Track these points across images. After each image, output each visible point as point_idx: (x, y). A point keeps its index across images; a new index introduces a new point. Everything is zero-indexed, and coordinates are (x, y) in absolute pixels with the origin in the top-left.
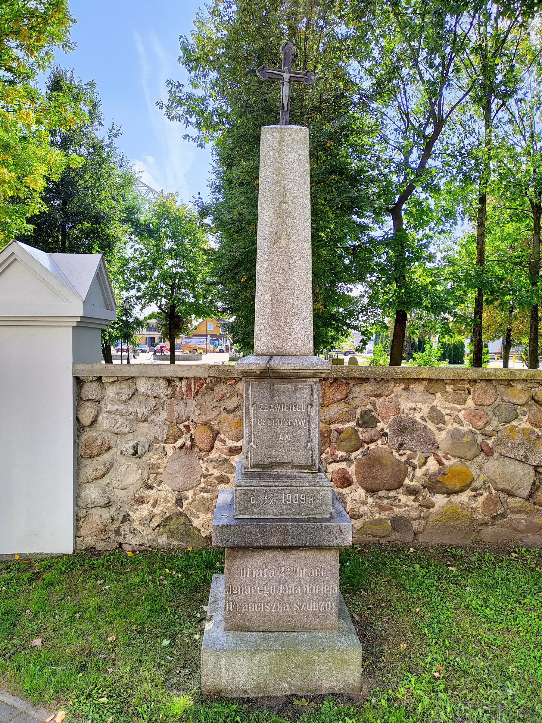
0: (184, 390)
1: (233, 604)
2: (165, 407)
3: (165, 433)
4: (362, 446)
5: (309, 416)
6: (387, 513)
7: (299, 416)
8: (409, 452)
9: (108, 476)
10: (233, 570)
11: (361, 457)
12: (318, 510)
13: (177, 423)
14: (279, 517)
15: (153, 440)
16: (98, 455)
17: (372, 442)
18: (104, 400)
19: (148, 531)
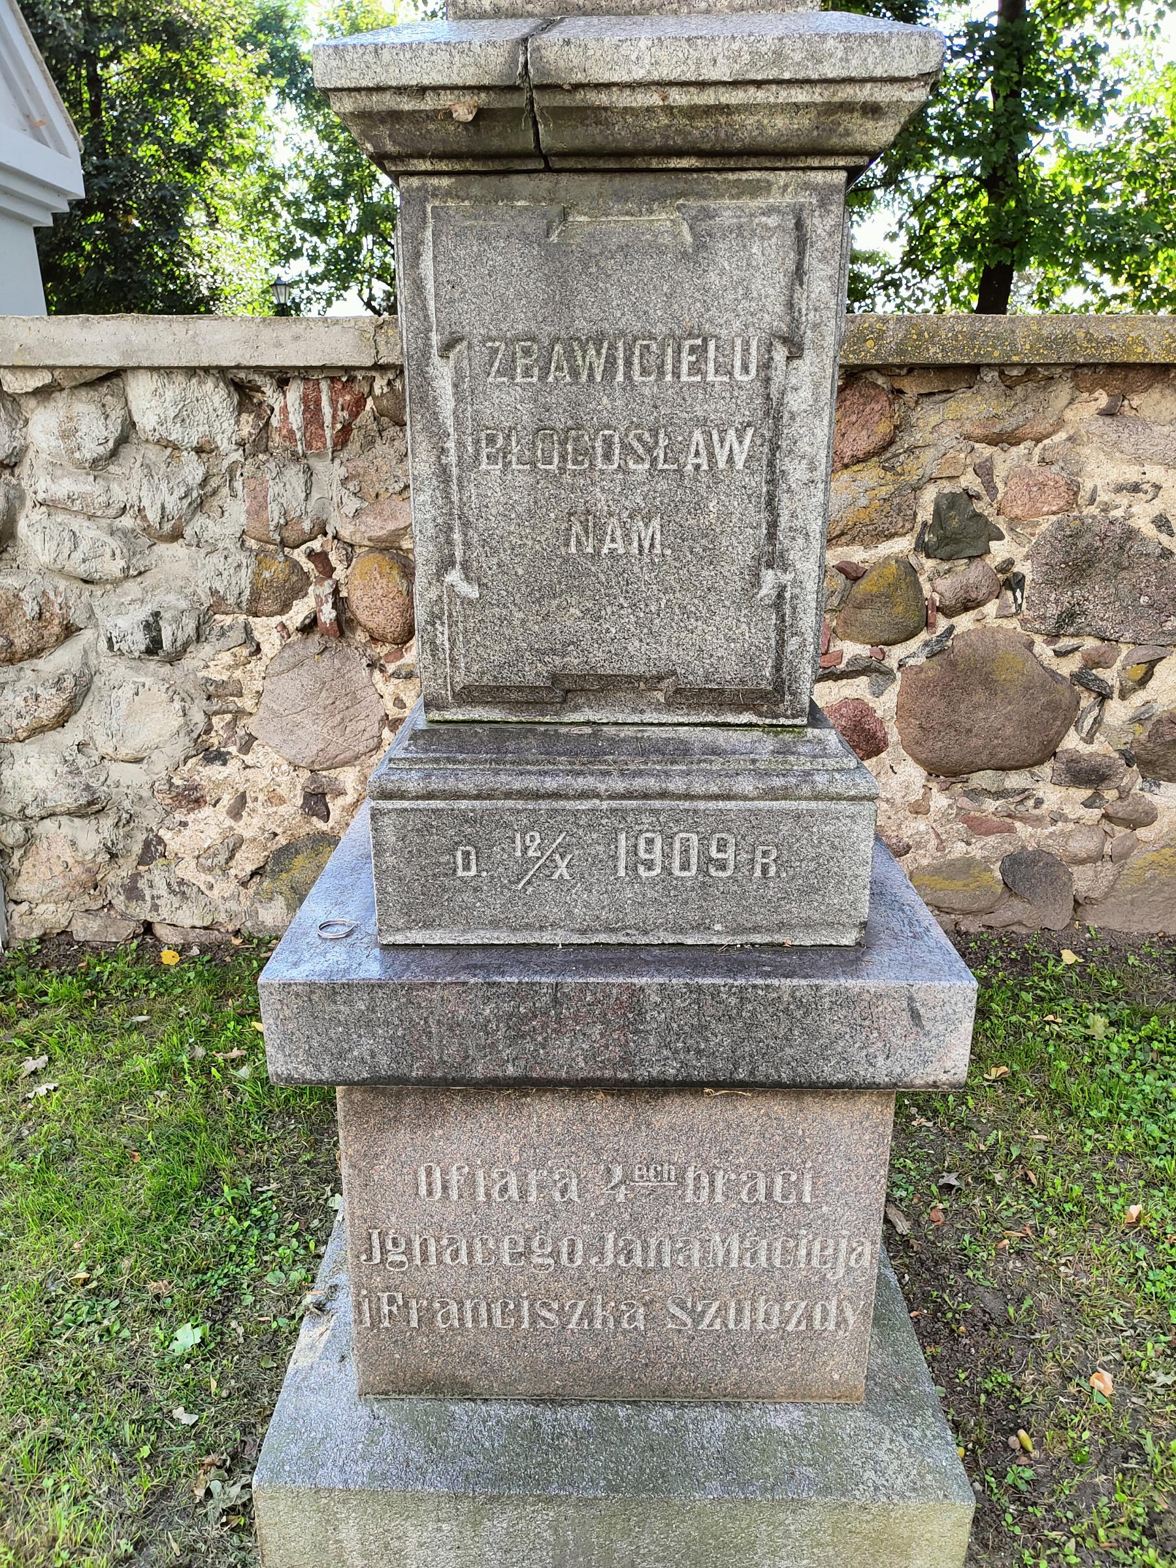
0: (296, 420)
1: (391, 1301)
2: (238, 485)
3: (244, 579)
4: (928, 624)
5: (774, 412)
6: (992, 840)
7: (713, 410)
8: (1090, 643)
9: (78, 720)
10: (382, 1171)
11: (921, 660)
12: (795, 910)
13: (283, 543)
14: (602, 938)
15: (207, 601)
16: (35, 653)
17: (966, 609)
18: (26, 462)
19: (224, 887)
